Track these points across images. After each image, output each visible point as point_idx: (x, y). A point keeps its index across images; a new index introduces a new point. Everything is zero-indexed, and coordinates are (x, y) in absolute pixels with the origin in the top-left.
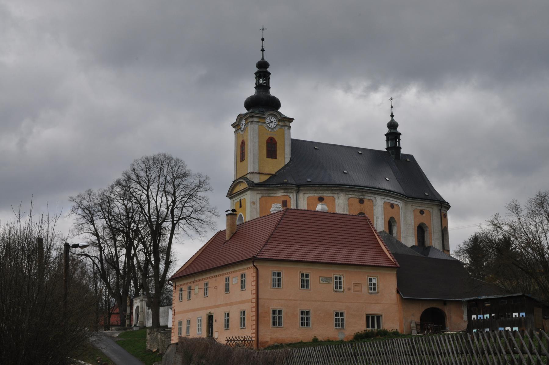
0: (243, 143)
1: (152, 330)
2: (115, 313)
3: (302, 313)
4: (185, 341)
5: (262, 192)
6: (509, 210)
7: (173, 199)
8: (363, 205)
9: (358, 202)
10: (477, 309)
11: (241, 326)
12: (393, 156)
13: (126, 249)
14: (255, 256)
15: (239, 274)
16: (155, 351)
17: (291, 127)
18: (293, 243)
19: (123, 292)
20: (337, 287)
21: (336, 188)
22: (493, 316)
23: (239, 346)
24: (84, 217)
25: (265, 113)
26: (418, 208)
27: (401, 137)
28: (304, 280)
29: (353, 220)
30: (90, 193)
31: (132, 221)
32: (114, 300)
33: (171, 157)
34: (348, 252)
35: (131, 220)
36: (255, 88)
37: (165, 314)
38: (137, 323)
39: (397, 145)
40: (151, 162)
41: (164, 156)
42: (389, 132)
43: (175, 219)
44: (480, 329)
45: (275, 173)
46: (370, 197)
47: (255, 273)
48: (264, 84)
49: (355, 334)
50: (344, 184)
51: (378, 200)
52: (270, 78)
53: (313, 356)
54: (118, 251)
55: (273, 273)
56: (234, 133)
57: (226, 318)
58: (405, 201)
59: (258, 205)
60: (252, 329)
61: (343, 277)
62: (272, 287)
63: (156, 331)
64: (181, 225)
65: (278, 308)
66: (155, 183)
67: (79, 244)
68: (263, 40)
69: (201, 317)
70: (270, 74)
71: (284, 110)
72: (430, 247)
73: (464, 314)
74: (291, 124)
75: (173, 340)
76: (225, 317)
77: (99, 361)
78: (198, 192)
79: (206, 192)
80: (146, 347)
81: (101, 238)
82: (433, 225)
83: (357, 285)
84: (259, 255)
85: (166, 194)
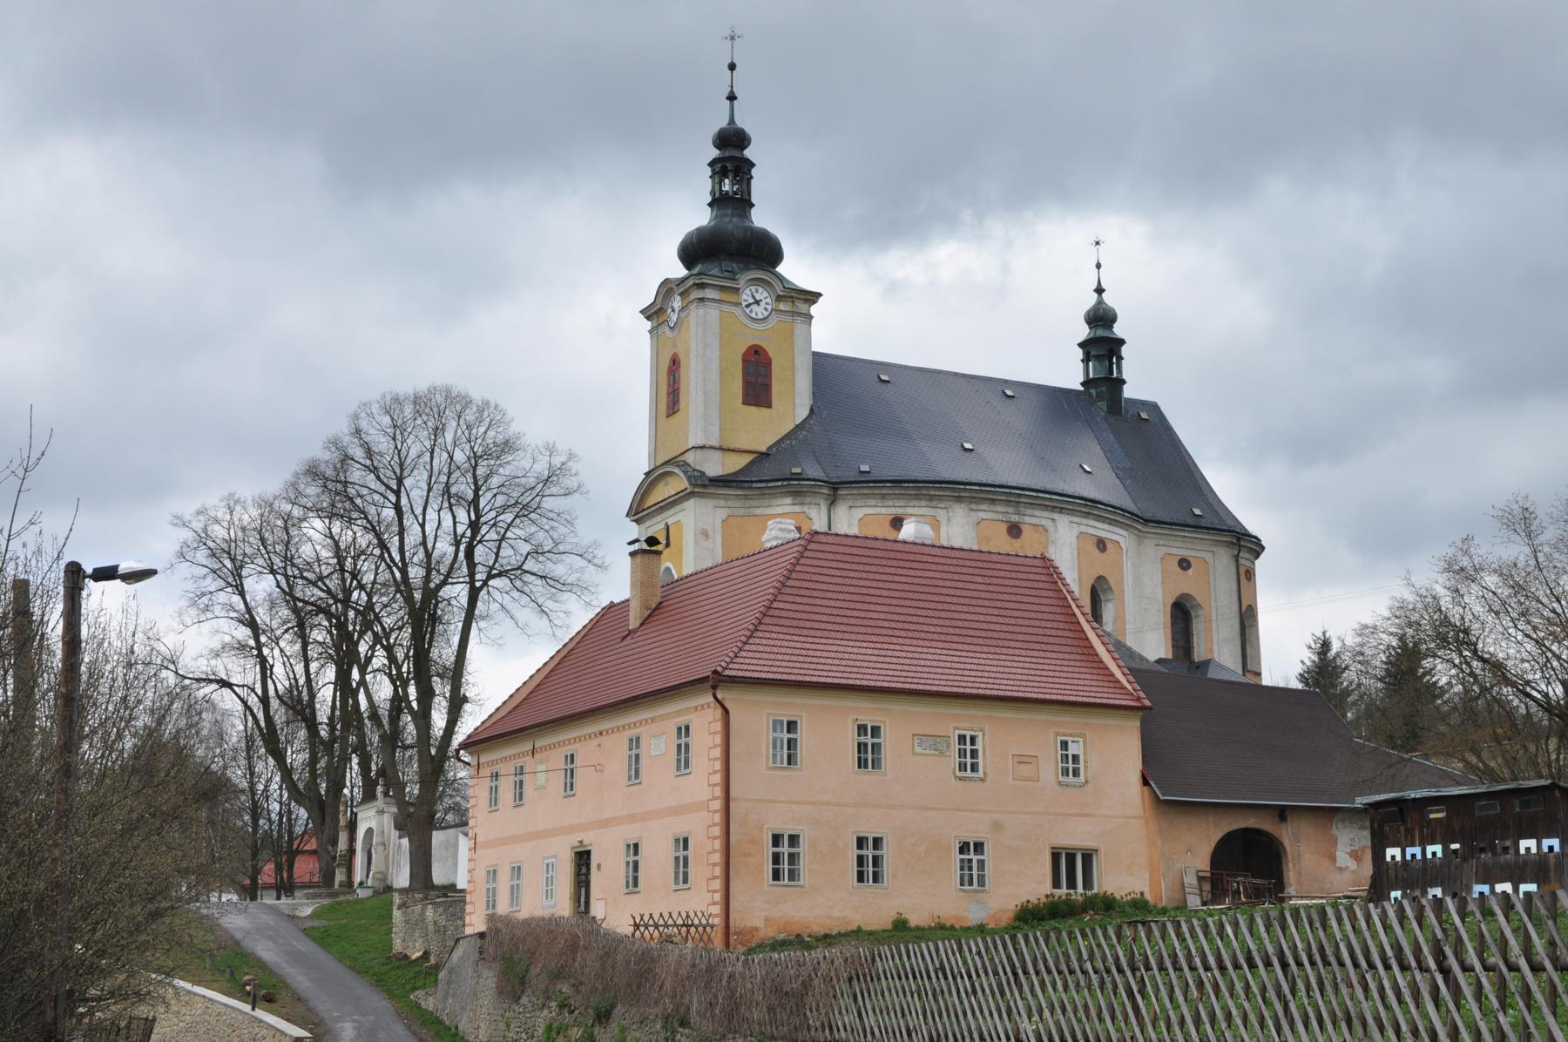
0: (675, 363)
1: (410, 896)
2: (307, 851)
3: (861, 842)
4: (507, 925)
5: (730, 503)
6: (1505, 527)
7: (473, 517)
8: (1019, 540)
10: (1402, 828)
11: (677, 883)
12: (1103, 405)
13: (336, 664)
14: (719, 669)
15: (671, 726)
16: (417, 959)
17: (812, 317)
18: (833, 635)
19: (327, 791)
20: (965, 765)
21: (942, 493)
22: (1455, 851)
23: (672, 942)
24: (215, 572)
25: (737, 277)
26: (1174, 551)
27: (1124, 350)
28: (866, 745)
29: (1010, 567)
30: (232, 504)
31: (355, 582)
32: (303, 813)
33: (465, 397)
34: (995, 663)
35: (351, 582)
36: (710, 205)
37: (447, 849)
38: (367, 877)
39: (1112, 374)
40: (408, 410)
41: (448, 391)
42: (1091, 336)
43: (478, 577)
44: (1412, 890)
45: (768, 449)
46: (1040, 517)
47: (719, 723)
48: (735, 193)
49: (1019, 908)
50: (964, 480)
51: (1060, 527)
52: (752, 177)
53: (956, 971)
54: (312, 671)
55: (775, 722)
56: (648, 335)
57: (631, 858)
58: (1137, 532)
59: (719, 541)
60: (709, 891)
61: (984, 735)
62: (771, 765)
63: (422, 900)
64: (496, 595)
65: (787, 830)
66: (418, 469)
67: (117, 567)
68: (732, 67)
69: (555, 856)
70: (753, 165)
71: (793, 269)
72: (1206, 664)
73: (1339, 846)
74: (814, 310)
75: (471, 925)
76: (628, 855)
77: (248, 988)
78: (545, 499)
79: (568, 497)
80: (389, 945)
81: (264, 632)
82: (1216, 602)
83: (1022, 760)
84: (730, 666)
85: (450, 503)
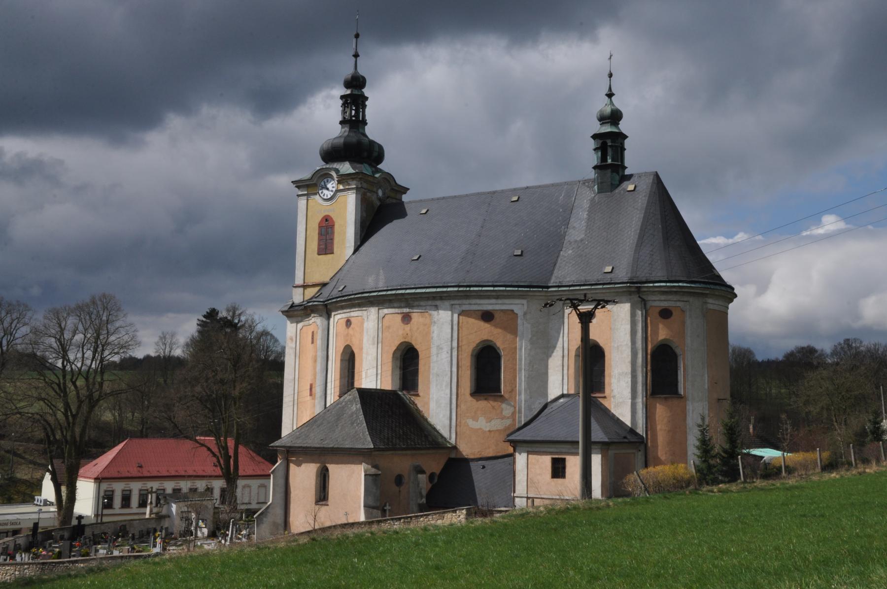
8: (409, 325)
9: (400, 321)
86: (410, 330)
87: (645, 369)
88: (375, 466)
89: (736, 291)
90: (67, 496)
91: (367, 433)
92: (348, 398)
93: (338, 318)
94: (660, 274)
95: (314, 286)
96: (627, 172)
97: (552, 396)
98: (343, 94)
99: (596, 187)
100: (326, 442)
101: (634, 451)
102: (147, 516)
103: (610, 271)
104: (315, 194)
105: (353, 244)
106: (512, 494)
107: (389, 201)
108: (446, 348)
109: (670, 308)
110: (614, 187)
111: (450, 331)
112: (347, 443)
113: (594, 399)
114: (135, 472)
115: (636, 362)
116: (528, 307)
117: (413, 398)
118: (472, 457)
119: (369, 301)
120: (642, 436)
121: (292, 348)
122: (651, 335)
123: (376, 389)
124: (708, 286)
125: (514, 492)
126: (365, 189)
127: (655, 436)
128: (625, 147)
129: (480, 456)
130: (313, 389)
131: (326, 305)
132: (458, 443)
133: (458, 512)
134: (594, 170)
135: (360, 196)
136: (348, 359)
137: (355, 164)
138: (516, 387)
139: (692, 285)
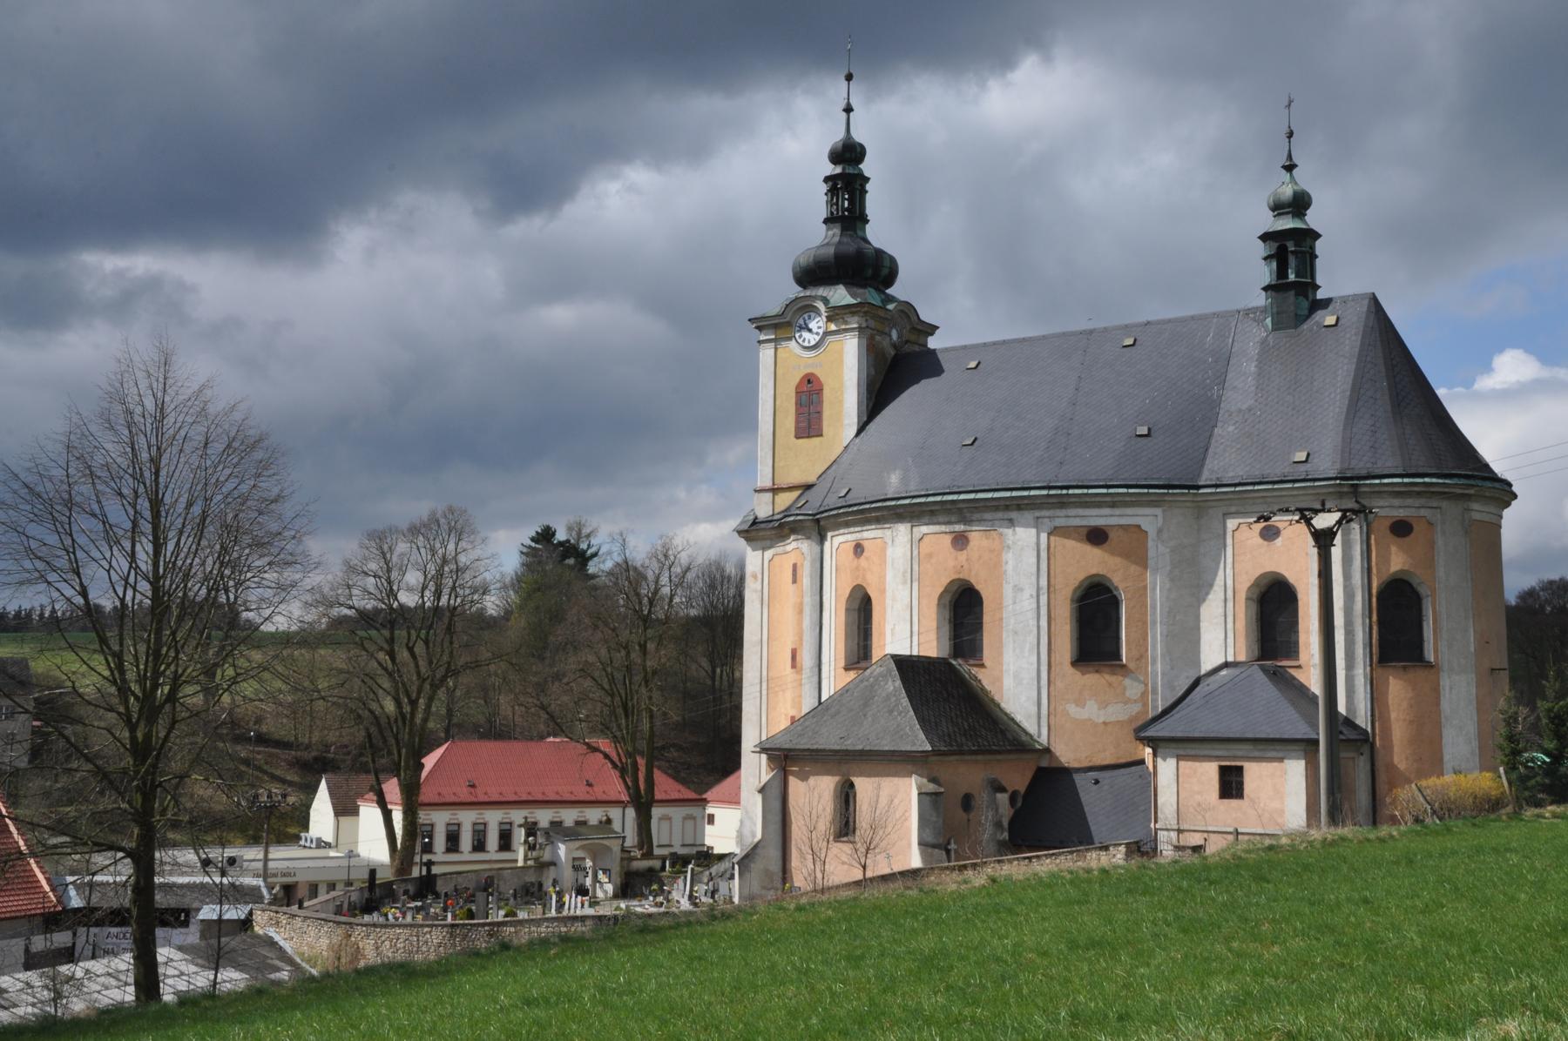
9: (950, 545)
86: (967, 560)
87: (1367, 621)
88: (933, 780)
89: (1514, 489)
90: (405, 827)
91: (918, 726)
92: (878, 670)
93: (839, 542)
94: (1389, 462)
95: (791, 489)
96: (1320, 295)
97: (1206, 666)
98: (828, 174)
99: (1269, 321)
100: (849, 742)
101: (1351, 755)
102: (520, 864)
103: (1304, 459)
104: (789, 339)
105: (856, 420)
106: (1152, 825)
107: (908, 348)
108: (1030, 591)
109: (1409, 520)
110: (1300, 319)
111: (1034, 560)
112: (884, 742)
113: (1281, 670)
114: (464, 794)
115: (1352, 609)
116: (1164, 518)
117: (974, 670)
118: (1075, 765)
119: (896, 514)
120: (1366, 731)
121: (756, 591)
122: (1377, 564)
123: (911, 656)
124: (1471, 482)
125: (1156, 822)
126: (873, 330)
127: (1386, 731)
128: (1317, 253)
129: (1091, 764)
130: (798, 658)
131: (818, 521)
132: (1052, 742)
133: (1111, 848)
134: (1264, 293)
135: (865, 341)
136: (857, 607)
137: (855, 289)
138: (1147, 650)
139: (1447, 481)
